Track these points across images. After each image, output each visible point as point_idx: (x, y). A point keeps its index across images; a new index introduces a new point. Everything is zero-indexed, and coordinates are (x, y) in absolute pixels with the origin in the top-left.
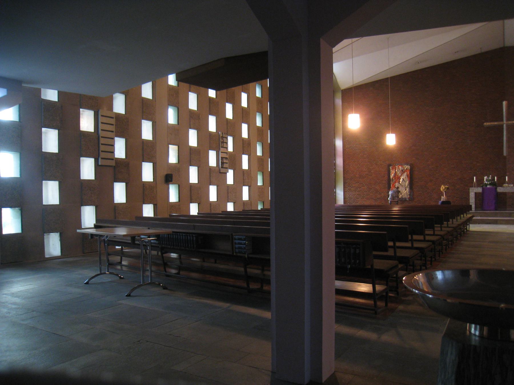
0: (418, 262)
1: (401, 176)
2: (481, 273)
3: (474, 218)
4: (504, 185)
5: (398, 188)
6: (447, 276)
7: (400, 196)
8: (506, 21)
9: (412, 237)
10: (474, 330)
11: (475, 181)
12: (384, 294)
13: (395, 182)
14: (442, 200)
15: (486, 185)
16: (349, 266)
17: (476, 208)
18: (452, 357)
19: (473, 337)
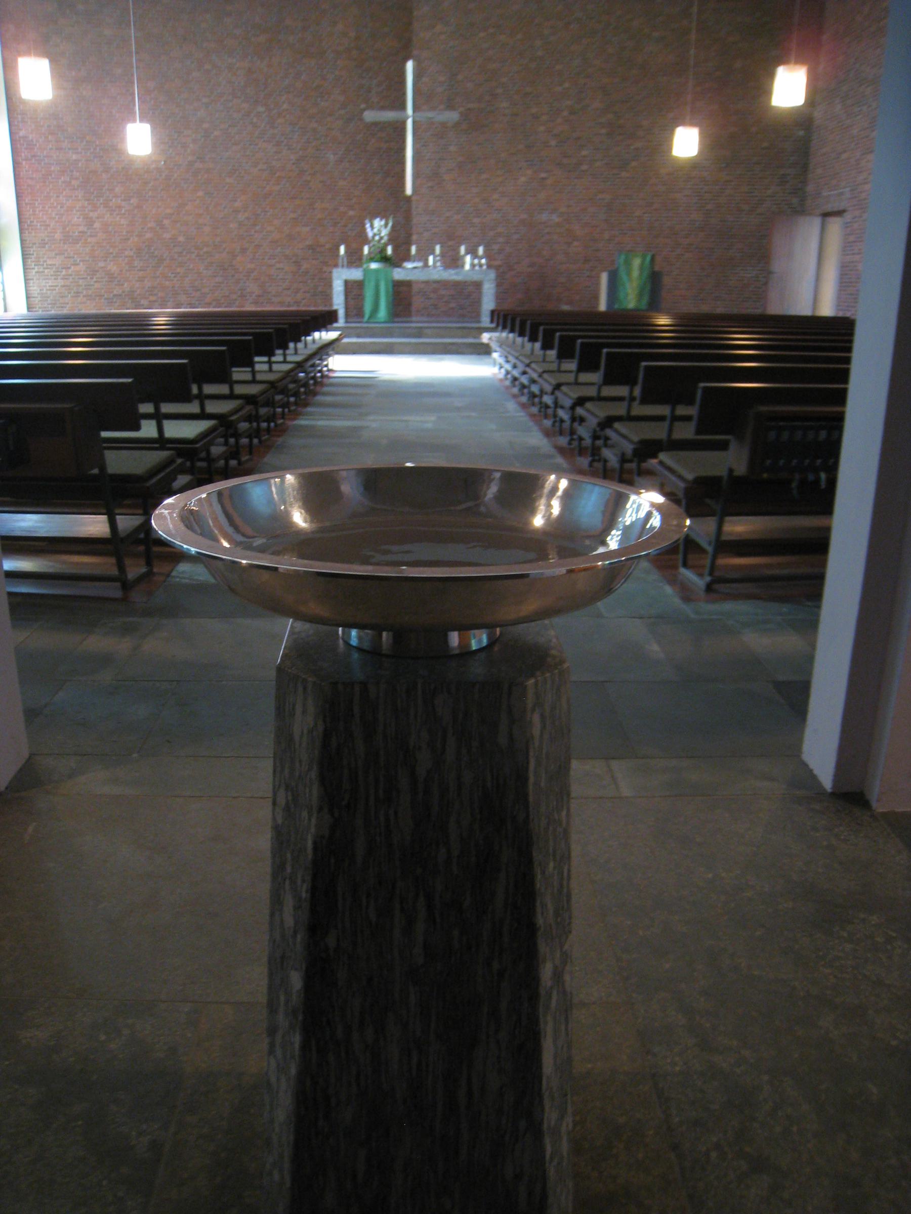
9: (200, 389)
12: (142, 536)
17: (347, 315)
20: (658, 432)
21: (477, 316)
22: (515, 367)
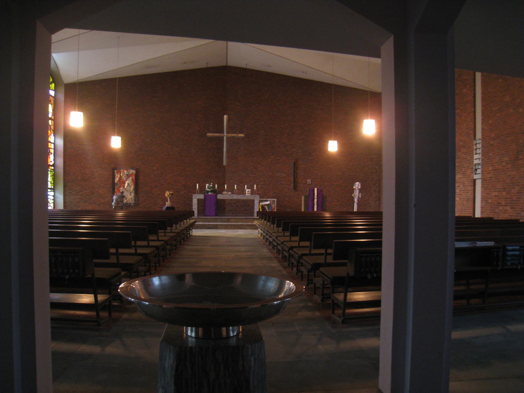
0: (142, 268)
1: (126, 180)
2: (196, 276)
3: (196, 223)
4: (224, 192)
5: (123, 192)
6: (164, 282)
7: (125, 201)
8: (229, 43)
9: (135, 243)
10: (190, 332)
11: (197, 188)
12: (108, 304)
13: (120, 187)
14: (166, 206)
15: (208, 192)
16: (67, 277)
17: (198, 213)
18: (170, 361)
19: (190, 339)
20: (321, 260)
21: (252, 214)
22: (267, 234)
